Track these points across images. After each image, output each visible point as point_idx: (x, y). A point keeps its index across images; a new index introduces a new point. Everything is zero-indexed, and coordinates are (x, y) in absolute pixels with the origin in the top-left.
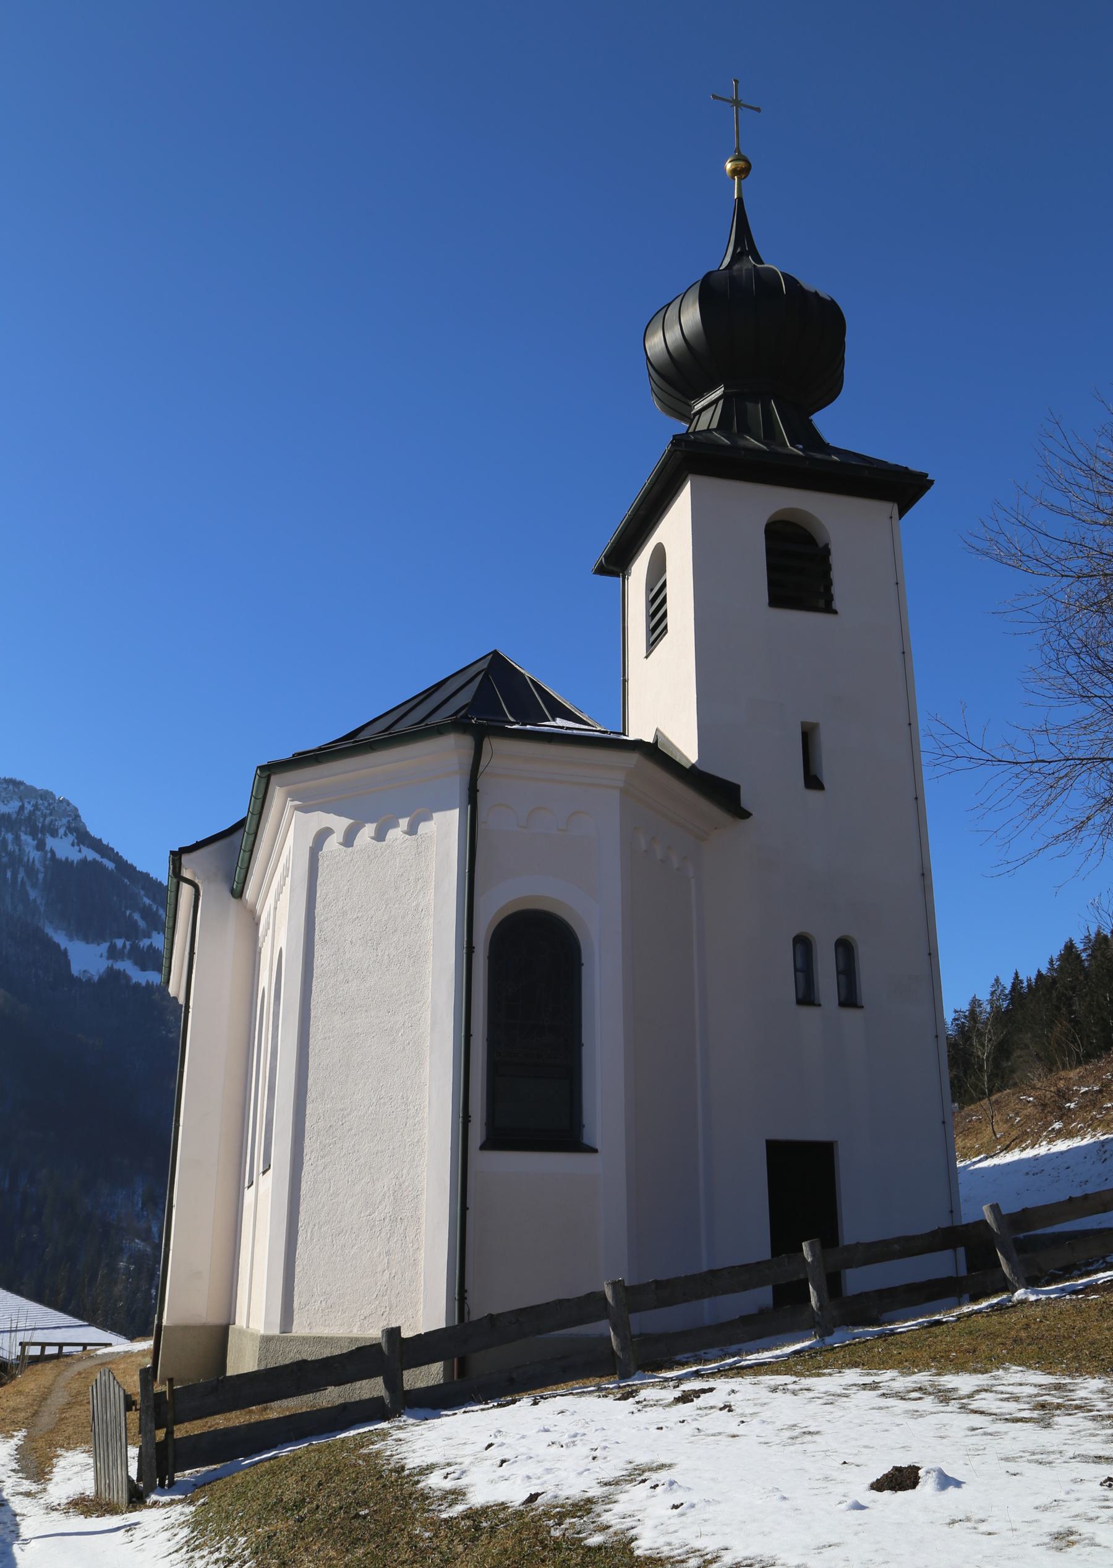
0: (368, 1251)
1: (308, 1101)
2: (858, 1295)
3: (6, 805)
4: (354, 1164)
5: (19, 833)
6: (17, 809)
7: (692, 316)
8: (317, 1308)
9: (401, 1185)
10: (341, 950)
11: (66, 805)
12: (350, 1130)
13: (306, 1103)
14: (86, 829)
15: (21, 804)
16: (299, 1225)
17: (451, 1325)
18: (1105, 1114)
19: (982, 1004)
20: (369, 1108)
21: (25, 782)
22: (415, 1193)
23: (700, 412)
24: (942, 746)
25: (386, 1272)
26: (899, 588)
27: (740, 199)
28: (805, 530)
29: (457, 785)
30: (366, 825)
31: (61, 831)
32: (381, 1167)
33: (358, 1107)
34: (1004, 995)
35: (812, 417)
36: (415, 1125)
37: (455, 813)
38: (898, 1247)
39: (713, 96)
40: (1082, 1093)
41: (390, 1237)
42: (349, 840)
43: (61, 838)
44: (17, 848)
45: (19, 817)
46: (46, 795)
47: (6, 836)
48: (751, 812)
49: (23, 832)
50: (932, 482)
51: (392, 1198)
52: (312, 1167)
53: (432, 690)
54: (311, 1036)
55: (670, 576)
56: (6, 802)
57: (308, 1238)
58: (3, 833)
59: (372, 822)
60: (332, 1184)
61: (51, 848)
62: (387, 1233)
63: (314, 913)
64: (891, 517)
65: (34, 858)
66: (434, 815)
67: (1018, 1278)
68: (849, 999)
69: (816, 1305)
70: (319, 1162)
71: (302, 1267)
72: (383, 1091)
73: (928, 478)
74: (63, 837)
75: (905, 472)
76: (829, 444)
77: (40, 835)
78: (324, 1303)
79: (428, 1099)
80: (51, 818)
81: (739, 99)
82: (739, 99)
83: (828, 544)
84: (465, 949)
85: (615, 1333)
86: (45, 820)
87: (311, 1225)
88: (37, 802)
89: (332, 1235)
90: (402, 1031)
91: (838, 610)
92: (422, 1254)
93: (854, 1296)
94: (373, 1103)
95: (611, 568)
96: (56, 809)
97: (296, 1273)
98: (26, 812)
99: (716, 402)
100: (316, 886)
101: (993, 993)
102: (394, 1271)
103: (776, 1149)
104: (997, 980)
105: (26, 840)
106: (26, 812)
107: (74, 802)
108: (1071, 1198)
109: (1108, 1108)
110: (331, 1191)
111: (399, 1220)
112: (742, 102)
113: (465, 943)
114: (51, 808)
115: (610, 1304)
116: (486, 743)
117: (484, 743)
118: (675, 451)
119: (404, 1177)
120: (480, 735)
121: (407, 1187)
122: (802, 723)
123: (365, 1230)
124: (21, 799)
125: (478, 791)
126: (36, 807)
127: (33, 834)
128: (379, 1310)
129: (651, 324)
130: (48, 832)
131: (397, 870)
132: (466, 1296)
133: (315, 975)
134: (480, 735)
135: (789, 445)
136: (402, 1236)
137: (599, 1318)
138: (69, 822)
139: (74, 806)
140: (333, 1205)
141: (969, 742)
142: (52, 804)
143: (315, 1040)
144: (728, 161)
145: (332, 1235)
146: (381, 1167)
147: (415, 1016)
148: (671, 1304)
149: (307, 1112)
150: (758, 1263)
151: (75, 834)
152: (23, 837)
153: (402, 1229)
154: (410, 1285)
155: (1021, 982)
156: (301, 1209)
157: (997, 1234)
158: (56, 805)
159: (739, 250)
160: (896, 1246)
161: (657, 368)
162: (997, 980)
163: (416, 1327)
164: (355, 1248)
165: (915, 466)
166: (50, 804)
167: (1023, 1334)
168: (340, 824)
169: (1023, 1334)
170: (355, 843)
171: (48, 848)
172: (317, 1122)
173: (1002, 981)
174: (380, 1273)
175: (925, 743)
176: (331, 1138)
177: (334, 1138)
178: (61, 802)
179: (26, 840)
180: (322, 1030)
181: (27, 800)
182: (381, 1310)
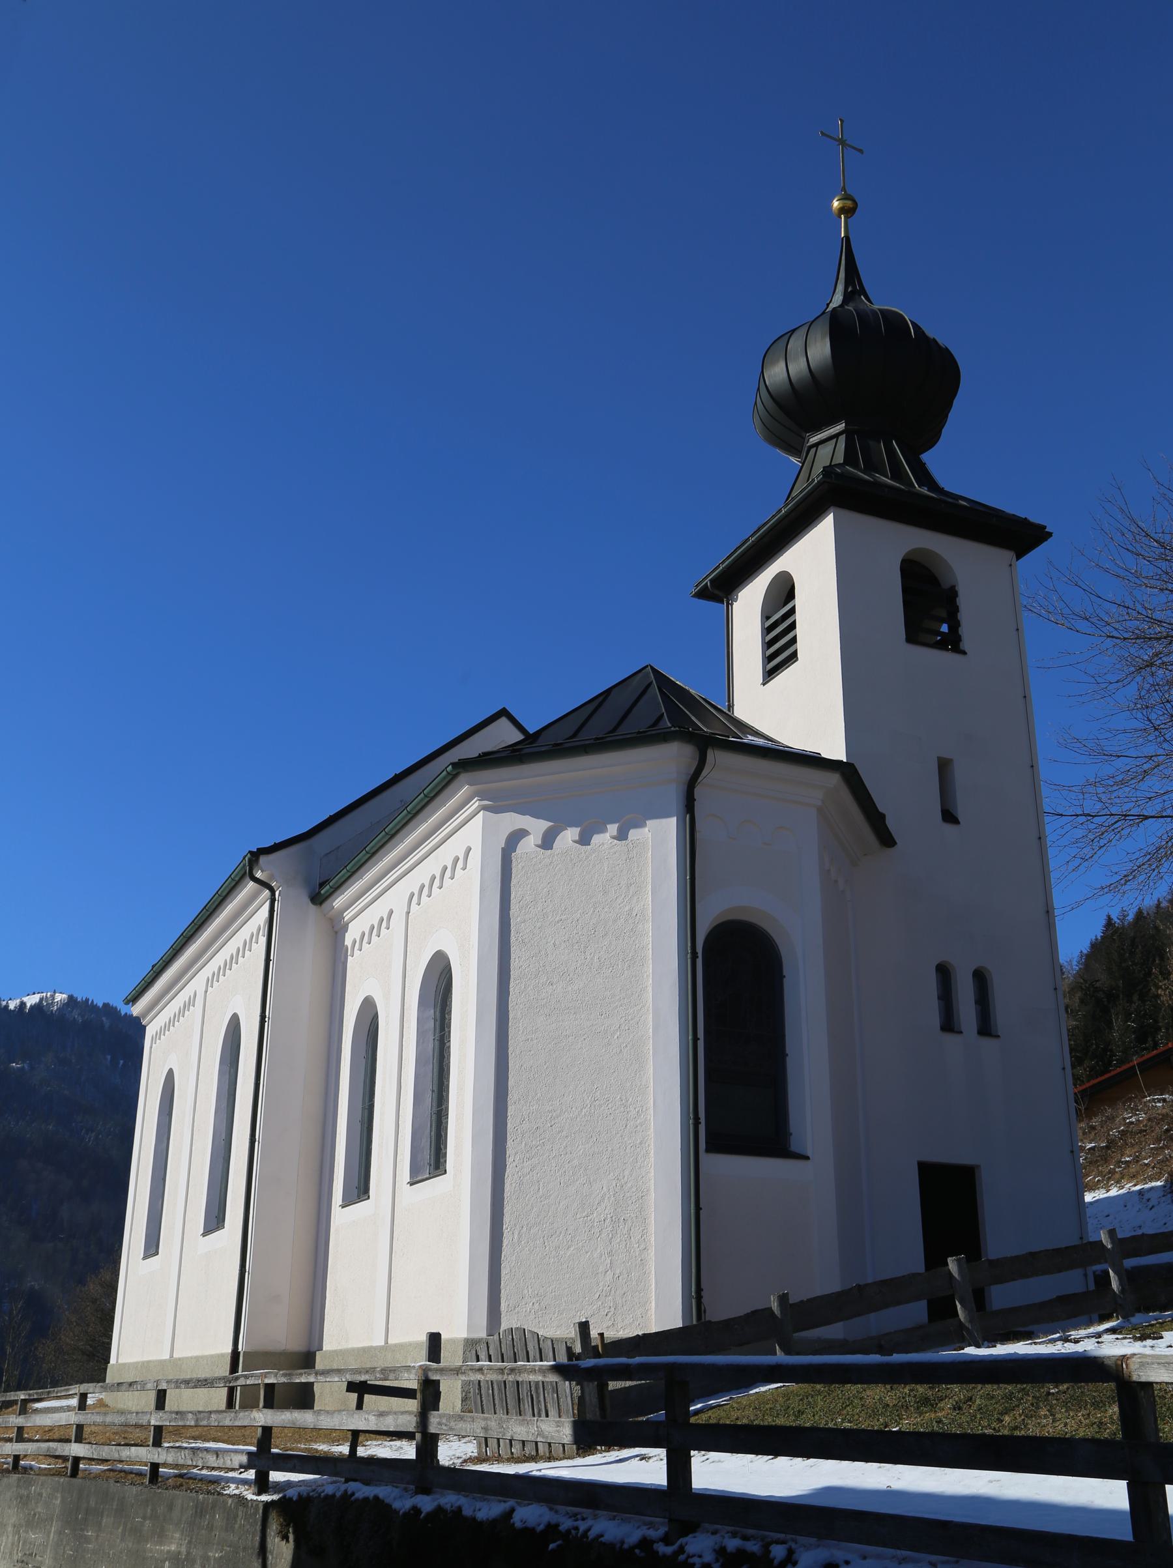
4: (567, 1166)
7: (821, 350)
13: (507, 1105)
16: (504, 1227)
17: (687, 1324)
18: (1125, 1168)
23: (817, 445)
25: (608, 1273)
27: (847, 238)
29: (673, 795)
37: (672, 822)
39: (822, 132)
40: (1089, 1149)
42: (547, 842)
50: (1050, 535)
57: (515, 1240)
66: (648, 822)
68: (986, 1029)
69: (1118, 1289)
71: (509, 1269)
72: (598, 1094)
73: (1046, 530)
75: (1025, 522)
76: (943, 488)
82: (845, 139)
87: (518, 1226)
91: (966, 651)
95: (716, 592)
99: (837, 436)
102: (618, 1272)
103: (927, 1171)
109: (1126, 1162)
113: (689, 948)
115: (956, 1278)
119: (626, 1178)
131: (605, 874)
135: (917, 486)
136: (626, 1236)
149: (509, 1114)
150: (1066, 1248)
153: (626, 1229)
154: (637, 1284)
156: (505, 1211)
159: (850, 289)
163: (645, 1326)
164: (572, 1249)
165: (1034, 519)
168: (537, 827)
174: (602, 1273)
176: (538, 1139)
180: (523, 1032)
182: (604, 1311)
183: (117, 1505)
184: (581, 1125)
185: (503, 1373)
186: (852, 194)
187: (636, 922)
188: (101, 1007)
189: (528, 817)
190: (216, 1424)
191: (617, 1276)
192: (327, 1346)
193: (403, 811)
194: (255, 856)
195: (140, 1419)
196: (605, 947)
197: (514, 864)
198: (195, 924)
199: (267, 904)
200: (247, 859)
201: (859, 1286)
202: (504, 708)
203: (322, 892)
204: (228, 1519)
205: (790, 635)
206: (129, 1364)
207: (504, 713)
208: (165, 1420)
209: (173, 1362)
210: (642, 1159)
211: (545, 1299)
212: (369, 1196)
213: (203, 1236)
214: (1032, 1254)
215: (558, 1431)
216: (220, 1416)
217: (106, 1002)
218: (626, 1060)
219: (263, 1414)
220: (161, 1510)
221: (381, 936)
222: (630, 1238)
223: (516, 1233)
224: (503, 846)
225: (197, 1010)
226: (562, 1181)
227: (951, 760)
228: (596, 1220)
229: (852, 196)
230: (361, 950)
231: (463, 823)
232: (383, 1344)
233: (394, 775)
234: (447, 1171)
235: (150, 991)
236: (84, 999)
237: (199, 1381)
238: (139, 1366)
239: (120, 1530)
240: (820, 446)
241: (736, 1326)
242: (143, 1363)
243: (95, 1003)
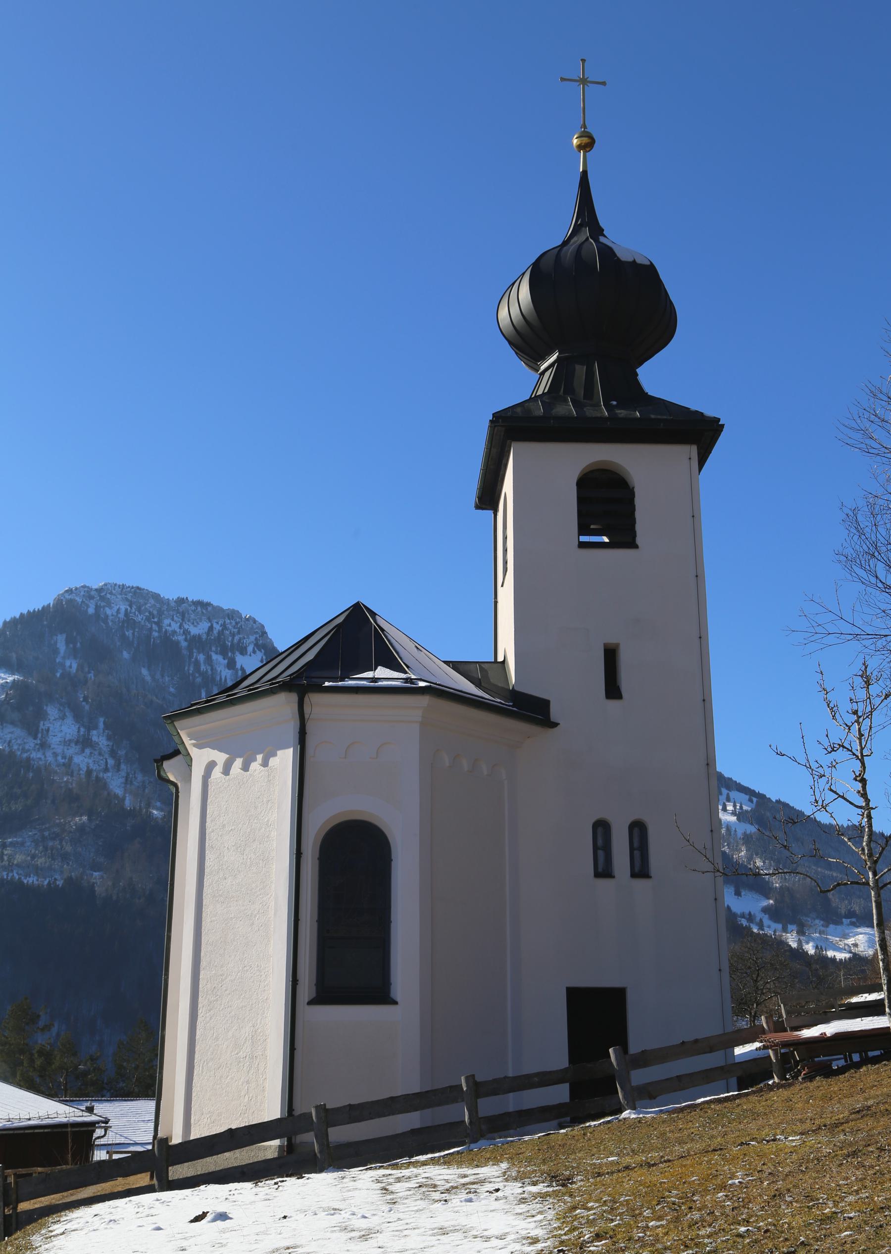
0: (236, 1081)
1: (201, 969)
2: (502, 1114)
3: (195, 626)
5: (210, 653)
6: (206, 630)
11: (252, 623)
12: (226, 990)
13: (199, 970)
14: (272, 644)
15: (210, 624)
21: (212, 603)
24: (815, 624)
27: (585, 174)
28: (618, 475)
30: (237, 759)
31: (250, 649)
32: (244, 1018)
35: (637, 370)
37: (290, 751)
41: (249, 1070)
42: (226, 771)
43: (250, 655)
44: (209, 668)
45: (209, 638)
46: (233, 614)
47: (198, 658)
48: (559, 722)
49: (214, 652)
51: (250, 1041)
52: (203, 1019)
53: (295, 647)
54: (203, 919)
56: (195, 624)
57: (200, 1072)
58: (195, 654)
59: (240, 757)
61: (241, 666)
62: (247, 1068)
63: (205, 826)
64: (690, 459)
65: (226, 676)
67: (627, 1102)
68: (641, 871)
70: (208, 1015)
74: (252, 653)
76: (647, 393)
77: (230, 654)
78: (209, 1119)
80: (239, 636)
81: (586, 77)
82: (586, 77)
85: (316, 1141)
86: (233, 639)
88: (225, 622)
91: (639, 545)
93: (499, 1115)
96: (243, 627)
97: (193, 1097)
98: (215, 632)
100: (207, 805)
102: (251, 1095)
105: (217, 659)
106: (215, 632)
107: (260, 619)
108: (683, 1043)
110: (214, 1036)
111: (254, 1057)
112: (588, 80)
113: (295, 851)
114: (238, 626)
116: (306, 699)
117: (305, 699)
121: (260, 1033)
122: (604, 644)
124: (210, 620)
126: (224, 626)
127: (224, 652)
129: (502, 299)
130: (238, 651)
133: (206, 873)
137: (308, 1131)
138: (256, 639)
139: (260, 623)
141: (842, 618)
142: (239, 622)
143: (205, 923)
144: (575, 137)
146: (244, 1018)
148: (359, 1121)
151: (262, 650)
152: (215, 657)
157: (616, 1069)
158: (243, 623)
160: (536, 1079)
161: (508, 338)
164: (228, 1078)
166: (237, 623)
168: (221, 757)
170: (230, 774)
171: (238, 666)
172: (206, 985)
177: (216, 996)
178: (248, 620)
179: (217, 659)
181: (215, 621)
186: (592, 133)
189: (216, 751)
197: (209, 787)
214: (392, 1098)
223: (201, 1067)
229: (590, 133)
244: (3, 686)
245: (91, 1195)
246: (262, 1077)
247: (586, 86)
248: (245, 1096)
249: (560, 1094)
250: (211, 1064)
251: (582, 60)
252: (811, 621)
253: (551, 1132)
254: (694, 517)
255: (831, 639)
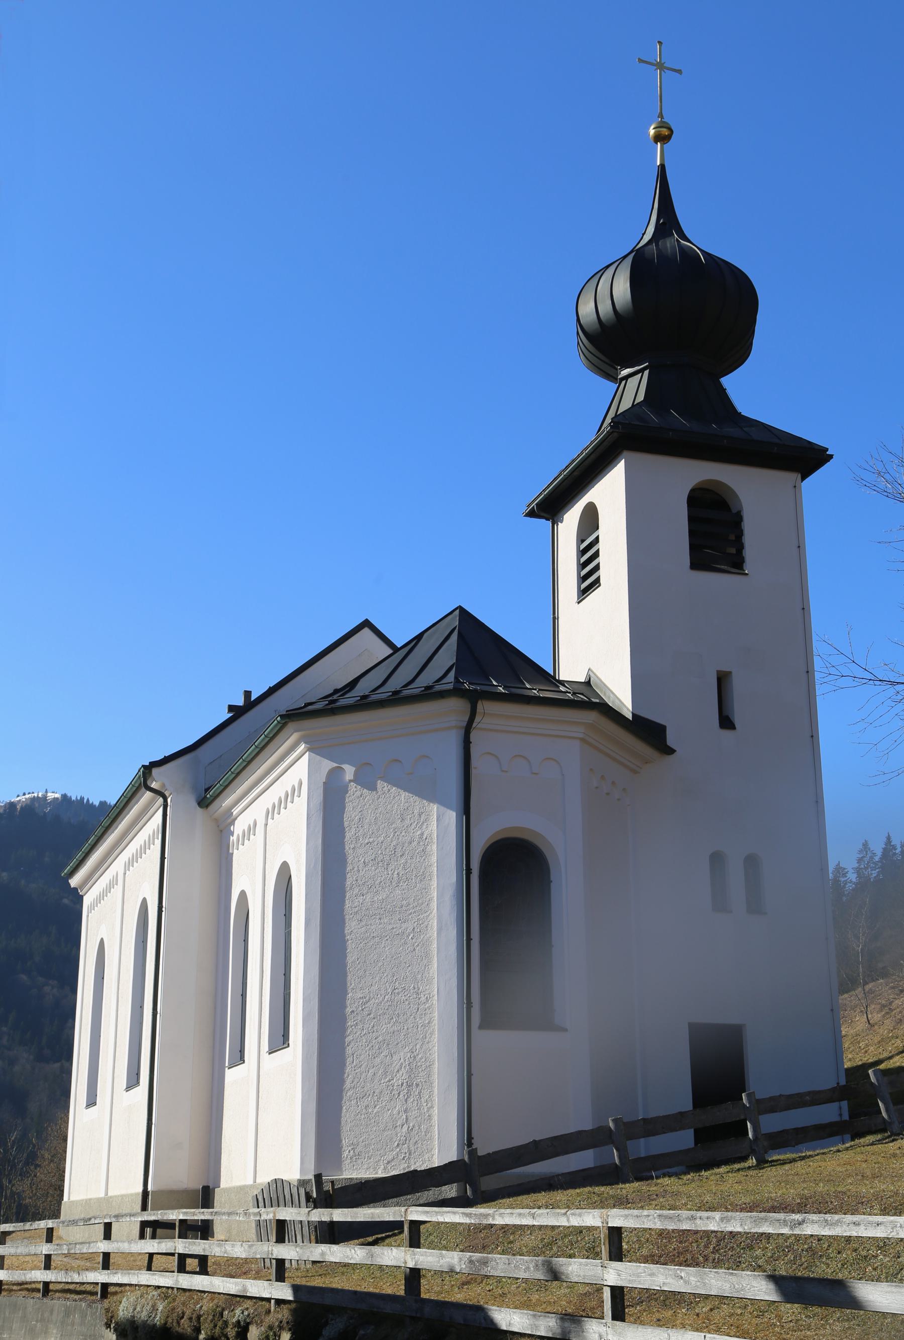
0: (388, 1110)
2: (781, 1131)
7: (622, 289)
8: (346, 1156)
9: (415, 1058)
10: (356, 869)
12: (369, 1014)
19: (847, 873)
20: (385, 996)
22: (428, 1064)
26: (801, 550)
27: (662, 167)
33: (376, 996)
34: (874, 863)
36: (426, 1010)
38: (809, 1099)
48: (676, 749)
55: (603, 532)
60: (355, 1057)
72: (397, 983)
73: (827, 453)
76: (741, 413)
79: (436, 989)
81: (662, 62)
82: (662, 62)
83: (741, 511)
84: (464, 871)
89: (357, 1098)
90: (412, 935)
92: (435, 1111)
93: (778, 1132)
94: (389, 993)
101: (860, 860)
102: (411, 1125)
104: (865, 845)
117: (478, 705)
118: (612, 432)
119: (417, 1051)
120: (473, 698)
121: (422, 1058)
122: (717, 671)
123: (385, 1093)
125: (471, 743)
128: (400, 1155)
132: (473, 1142)
134: (473, 698)
136: (417, 1097)
140: (356, 1074)
144: (652, 127)
145: (357, 1098)
147: (422, 923)
153: (418, 1091)
155: (894, 848)
160: (808, 1097)
161: (585, 328)
162: (865, 845)
164: (378, 1107)
167: (898, 1152)
169: (898, 1152)
173: (872, 846)
174: (399, 1126)
175: (818, 664)
176: (353, 1020)
182: (401, 1156)
183: (22, 1314)
184: (384, 1009)
185: (212, 1215)
187: (426, 844)
188: (97, 806)
190: (79, 1252)
191: (411, 1128)
192: (224, 1184)
193: (261, 736)
194: (147, 770)
195: (37, 1250)
196: (402, 865)
198: (110, 817)
199: (161, 810)
200: (141, 771)
201: (535, 1141)
202: (367, 619)
203: (208, 796)
204: (82, 1318)
205: (584, 572)
206: (77, 1202)
207: (367, 624)
208: (51, 1250)
209: (107, 1199)
210: (430, 1036)
211: (358, 1147)
212: (289, 1044)
213: (127, 1091)
215: (232, 1250)
216: (81, 1246)
217: (103, 800)
218: (418, 956)
219: (103, 1244)
220: (46, 1315)
221: (245, 845)
222: (421, 1098)
224: (324, 781)
225: (118, 889)
226: (370, 1054)
227: (730, 673)
228: (396, 1084)
230: (279, 814)
231: (249, 803)
232: (252, 1183)
233: (268, 687)
234: (245, 1061)
235: (77, 875)
236: (79, 798)
237: (70, 1221)
238: (84, 1203)
239: (23, 1332)
240: (629, 380)
241: (436, 1173)
242: (86, 1200)
243: (91, 802)
244: (456, 682)
245: (573, 1168)
246: (427, 1105)
247: (662, 71)
248: (403, 1126)
249: (684, 1139)
250: (352, 1092)
251: (659, 42)
252: (825, 662)
253: (379, 1236)
254: (800, 547)
255: (848, 682)
